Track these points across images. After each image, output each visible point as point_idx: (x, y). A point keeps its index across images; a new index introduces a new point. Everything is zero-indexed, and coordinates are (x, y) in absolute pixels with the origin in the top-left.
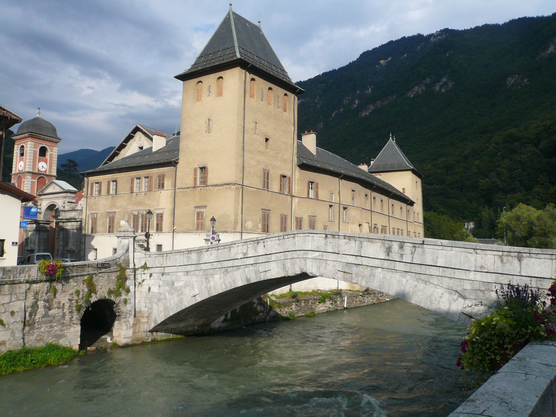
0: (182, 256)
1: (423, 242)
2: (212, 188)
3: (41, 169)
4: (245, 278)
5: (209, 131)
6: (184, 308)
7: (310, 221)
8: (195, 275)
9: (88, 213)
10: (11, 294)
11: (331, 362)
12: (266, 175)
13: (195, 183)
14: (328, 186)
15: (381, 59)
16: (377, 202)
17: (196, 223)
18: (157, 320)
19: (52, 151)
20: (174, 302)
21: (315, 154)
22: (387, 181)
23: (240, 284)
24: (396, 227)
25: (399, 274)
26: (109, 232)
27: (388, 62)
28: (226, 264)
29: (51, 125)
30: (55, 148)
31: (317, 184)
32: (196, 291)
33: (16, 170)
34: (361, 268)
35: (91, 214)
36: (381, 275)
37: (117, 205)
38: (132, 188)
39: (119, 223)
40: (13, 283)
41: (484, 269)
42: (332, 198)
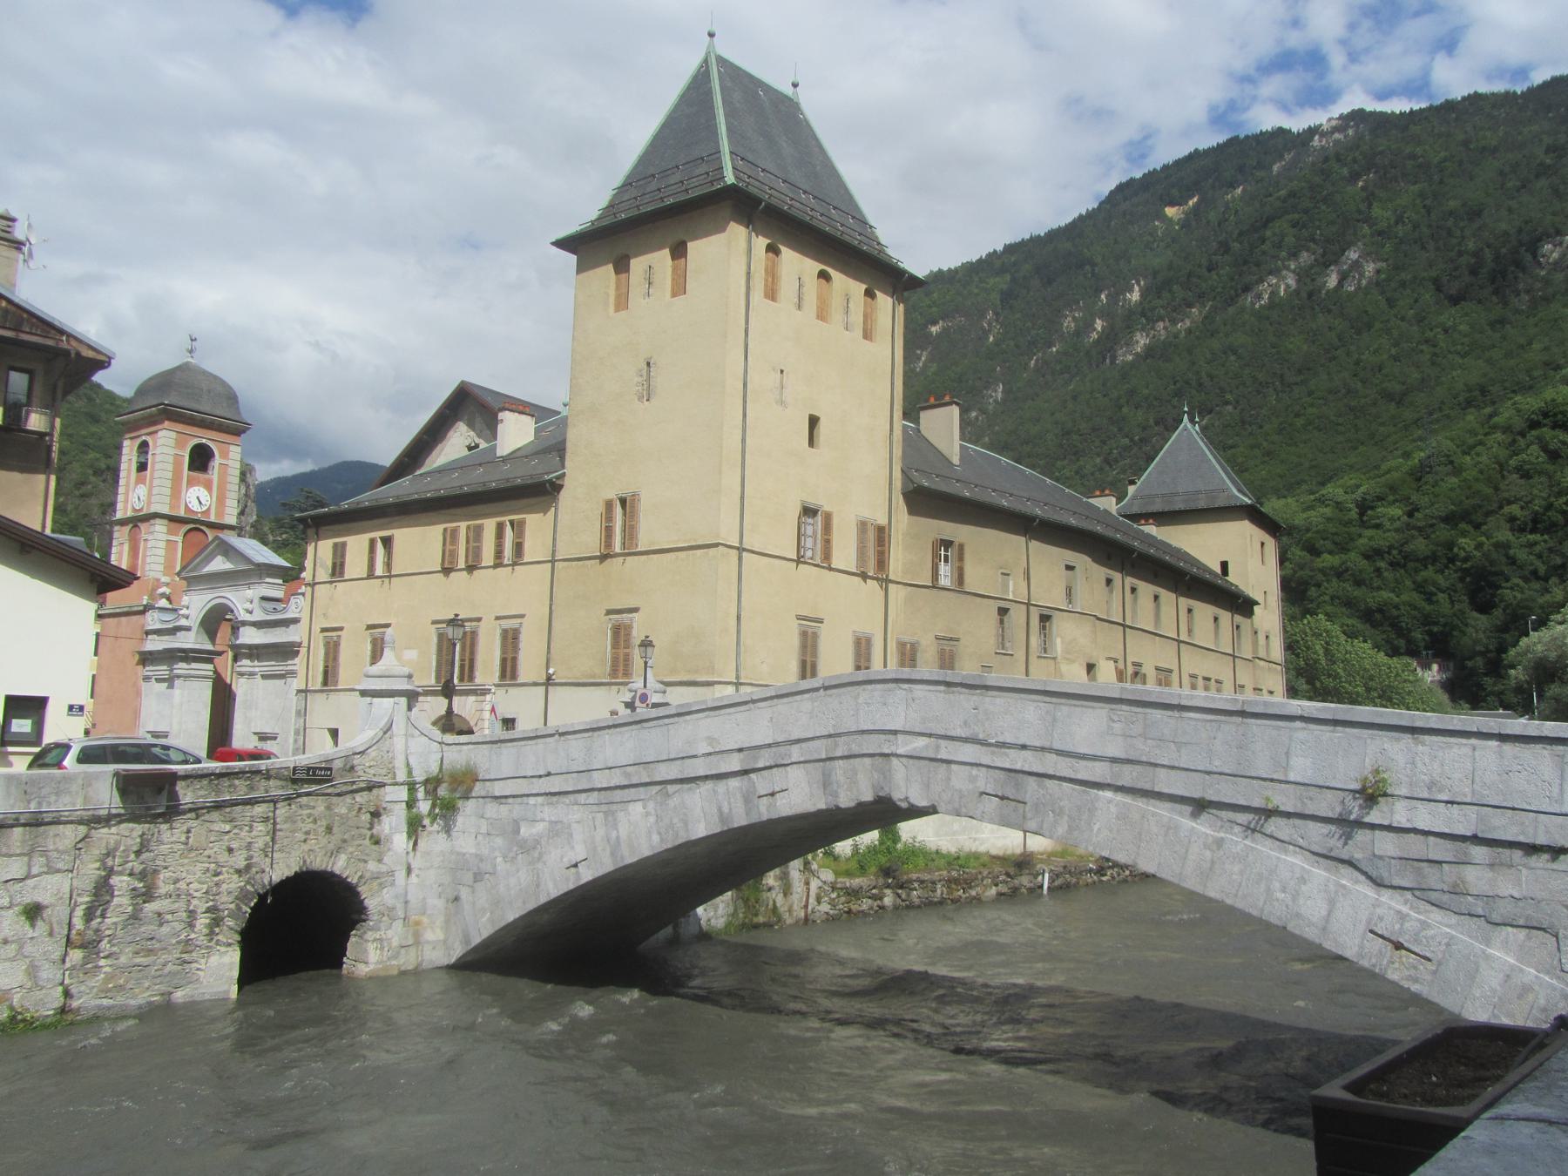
3: (195, 506)
5: (647, 394)
7: (942, 653)
10: (30, 854)
11: (1395, 1043)
14: (993, 555)
15: (1172, 204)
16: (1243, 639)
17: (609, 656)
19: (225, 455)
21: (956, 460)
22: (1175, 543)
23: (700, 830)
24: (1201, 673)
28: (665, 772)
29: (224, 383)
30: (232, 448)
31: (961, 547)
32: (579, 852)
33: (126, 508)
40: (36, 822)
41: (1440, 791)
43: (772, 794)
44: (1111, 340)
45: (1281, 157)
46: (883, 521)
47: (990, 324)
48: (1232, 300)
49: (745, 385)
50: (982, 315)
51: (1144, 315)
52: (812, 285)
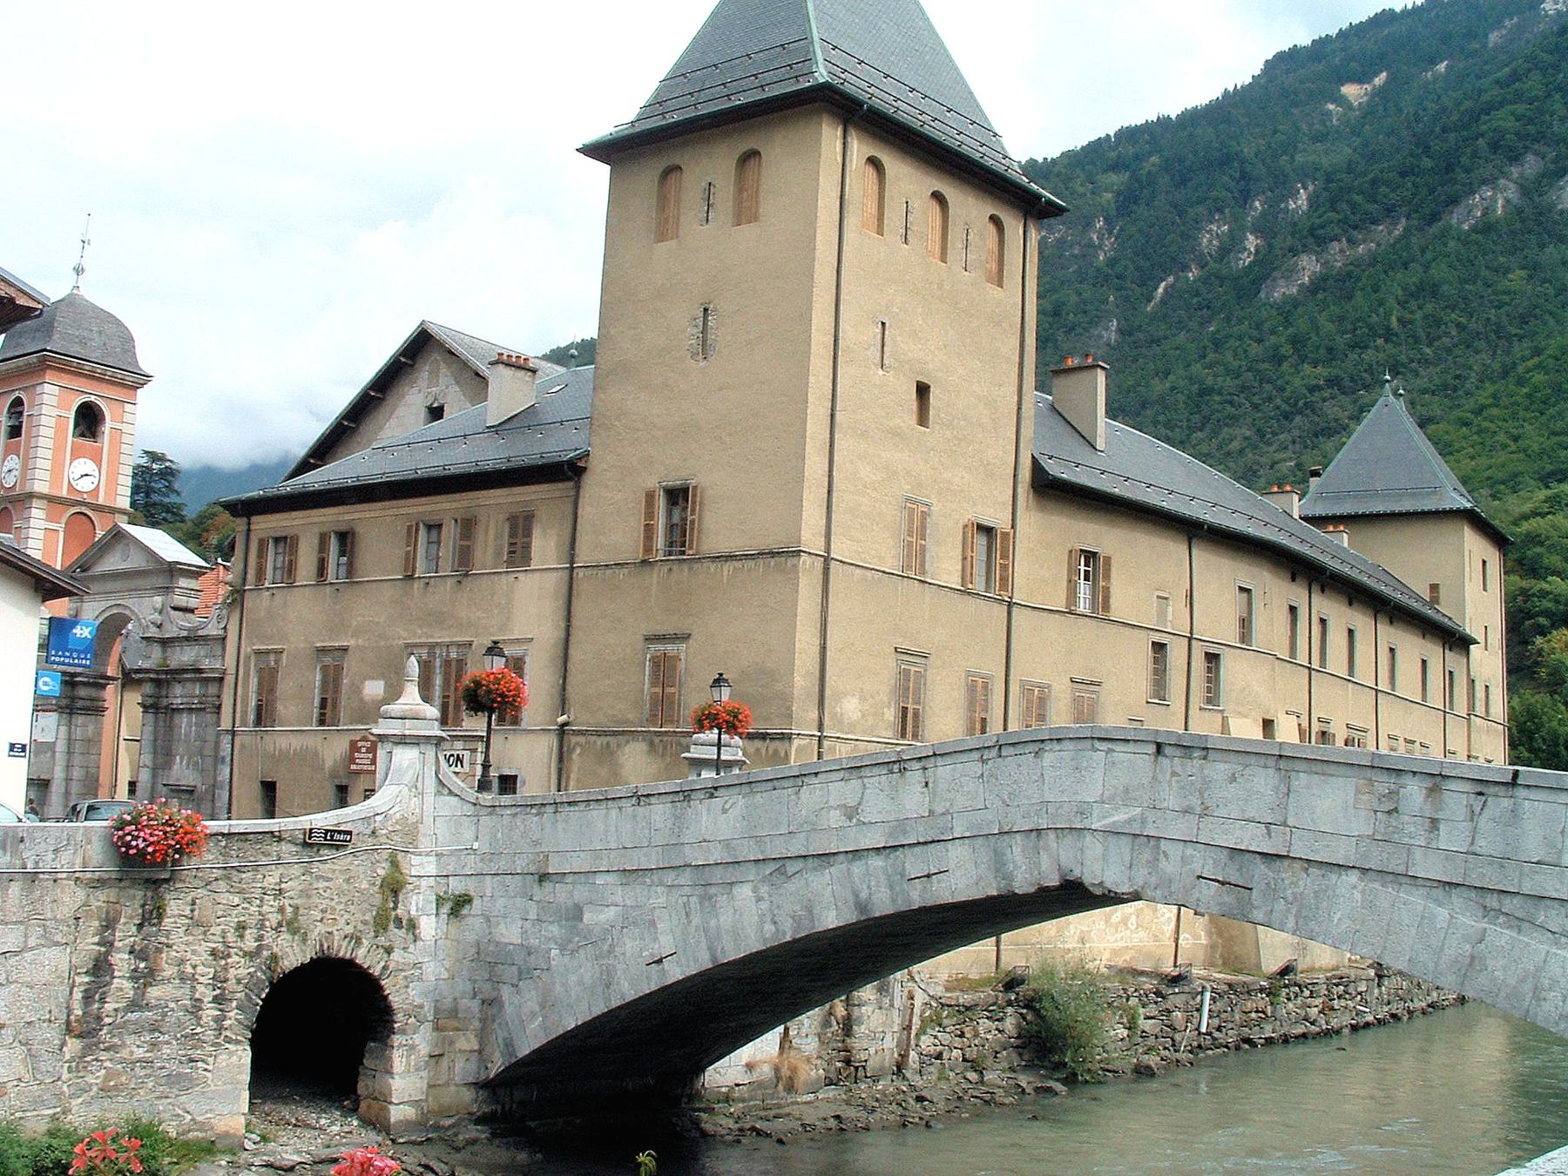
0: (614, 813)
1: (1516, 774)
2: (713, 567)
4: (851, 899)
5: (704, 348)
6: (616, 1003)
7: (1077, 701)
8: (661, 884)
9: (246, 649)
12: (917, 525)
13: (648, 549)
18: (517, 1043)
20: (581, 982)
23: (830, 919)
25: (1422, 891)
26: (322, 722)
27: (1380, 93)
31: (1108, 560)
32: (666, 944)
34: (1286, 873)
35: (258, 653)
36: (1357, 896)
37: (354, 624)
38: (410, 561)
39: (357, 690)
42: (1162, 614)
43: (928, 876)
44: (1265, 267)
45: (1498, 23)
46: (1008, 529)
47: (1100, 238)
48: (1434, 217)
49: (836, 340)
50: (1088, 225)
51: (1314, 237)
52: (861, 181)
